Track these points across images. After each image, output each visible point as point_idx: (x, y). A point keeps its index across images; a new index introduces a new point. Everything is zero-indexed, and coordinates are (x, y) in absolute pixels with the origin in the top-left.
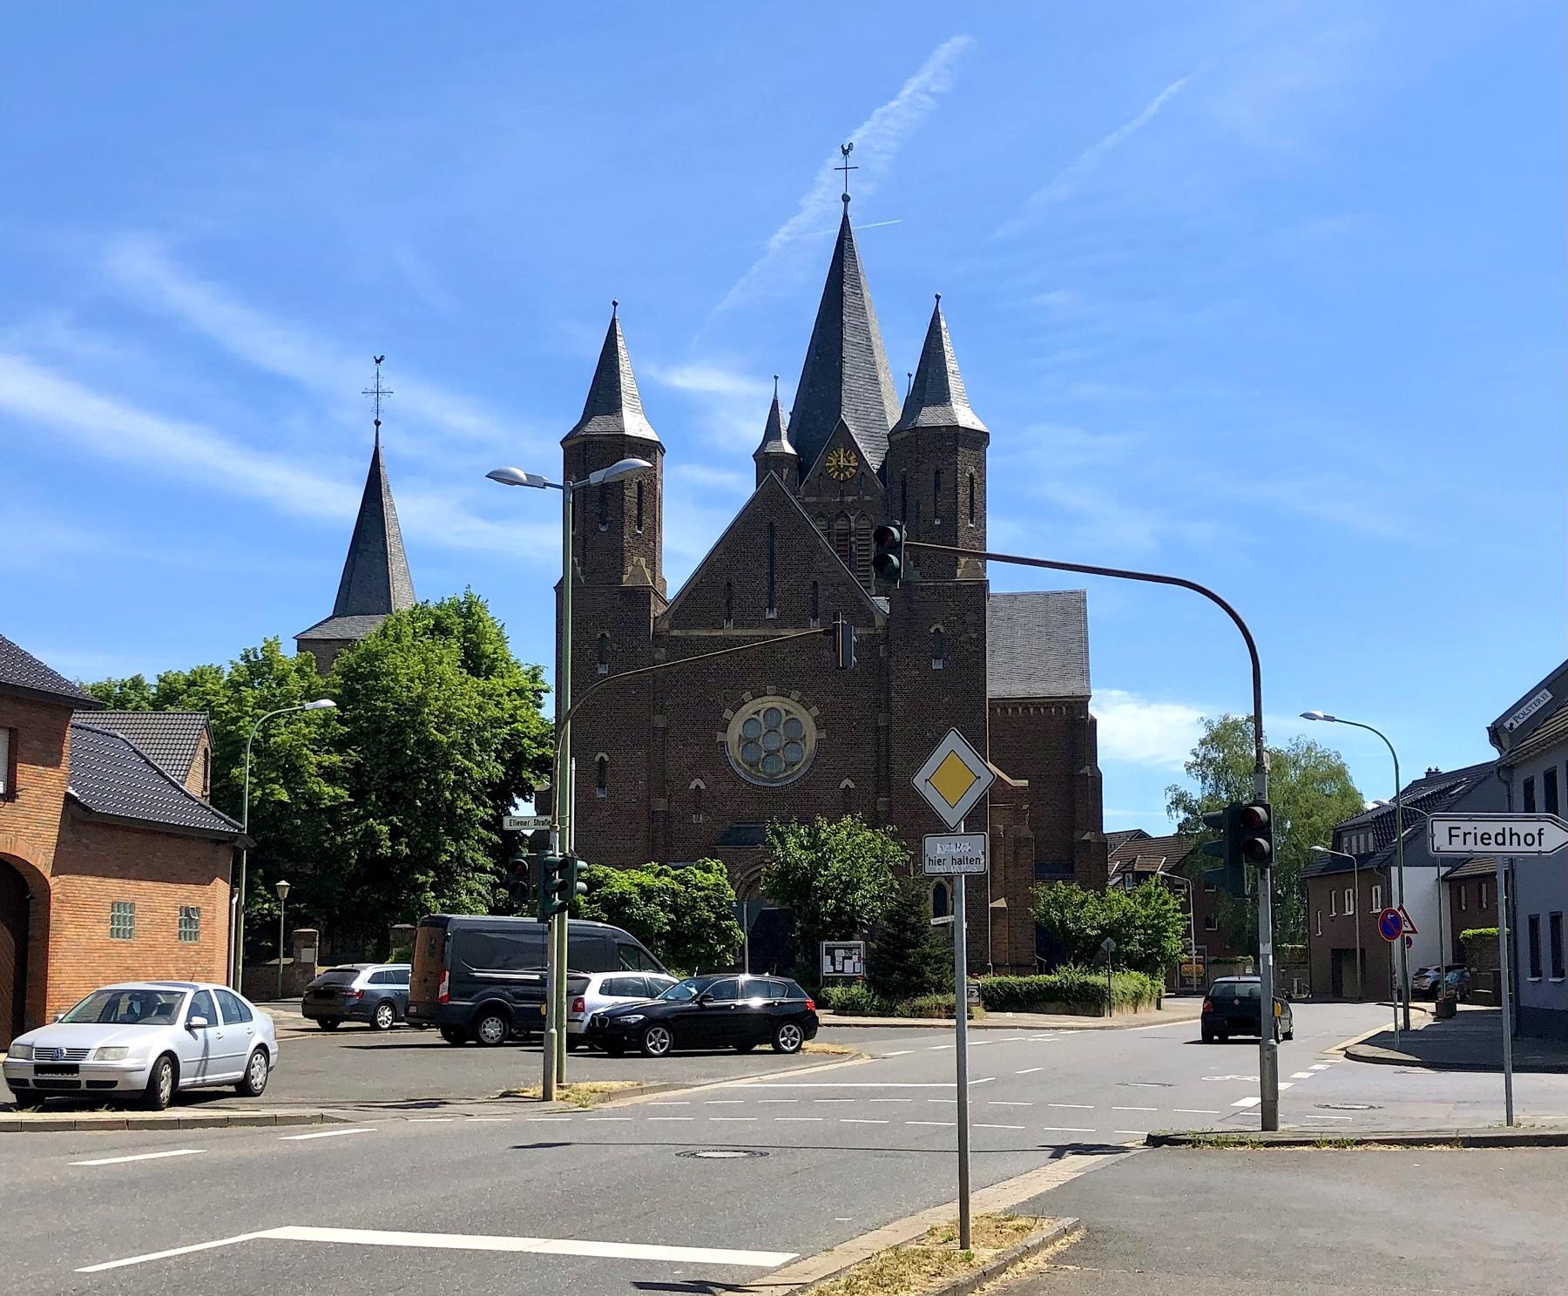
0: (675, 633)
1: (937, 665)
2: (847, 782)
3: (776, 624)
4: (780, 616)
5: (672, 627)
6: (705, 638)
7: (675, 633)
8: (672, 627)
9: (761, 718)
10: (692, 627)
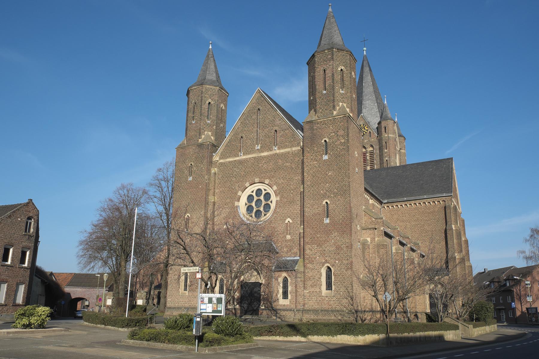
0: (221, 161)
1: (326, 157)
2: (289, 219)
3: (260, 151)
4: (261, 147)
5: (220, 159)
6: (232, 162)
7: (221, 161)
8: (220, 159)
9: (254, 194)
10: (227, 157)
